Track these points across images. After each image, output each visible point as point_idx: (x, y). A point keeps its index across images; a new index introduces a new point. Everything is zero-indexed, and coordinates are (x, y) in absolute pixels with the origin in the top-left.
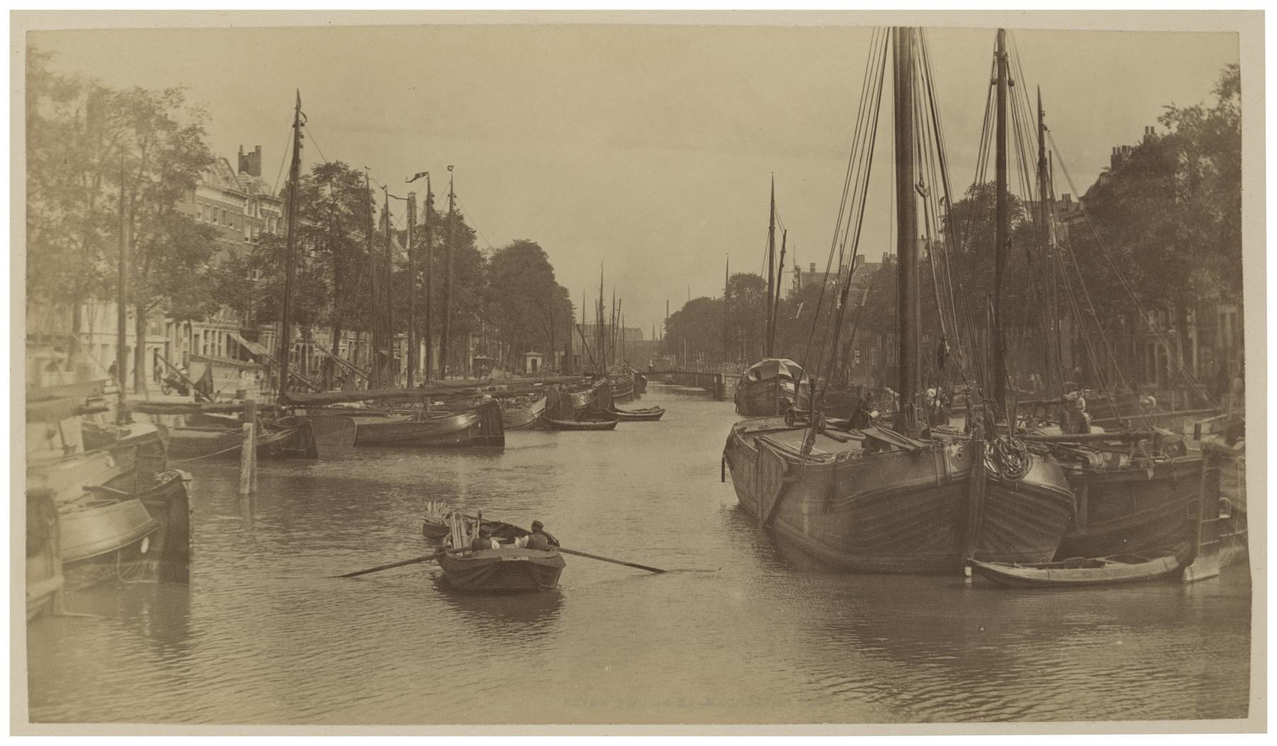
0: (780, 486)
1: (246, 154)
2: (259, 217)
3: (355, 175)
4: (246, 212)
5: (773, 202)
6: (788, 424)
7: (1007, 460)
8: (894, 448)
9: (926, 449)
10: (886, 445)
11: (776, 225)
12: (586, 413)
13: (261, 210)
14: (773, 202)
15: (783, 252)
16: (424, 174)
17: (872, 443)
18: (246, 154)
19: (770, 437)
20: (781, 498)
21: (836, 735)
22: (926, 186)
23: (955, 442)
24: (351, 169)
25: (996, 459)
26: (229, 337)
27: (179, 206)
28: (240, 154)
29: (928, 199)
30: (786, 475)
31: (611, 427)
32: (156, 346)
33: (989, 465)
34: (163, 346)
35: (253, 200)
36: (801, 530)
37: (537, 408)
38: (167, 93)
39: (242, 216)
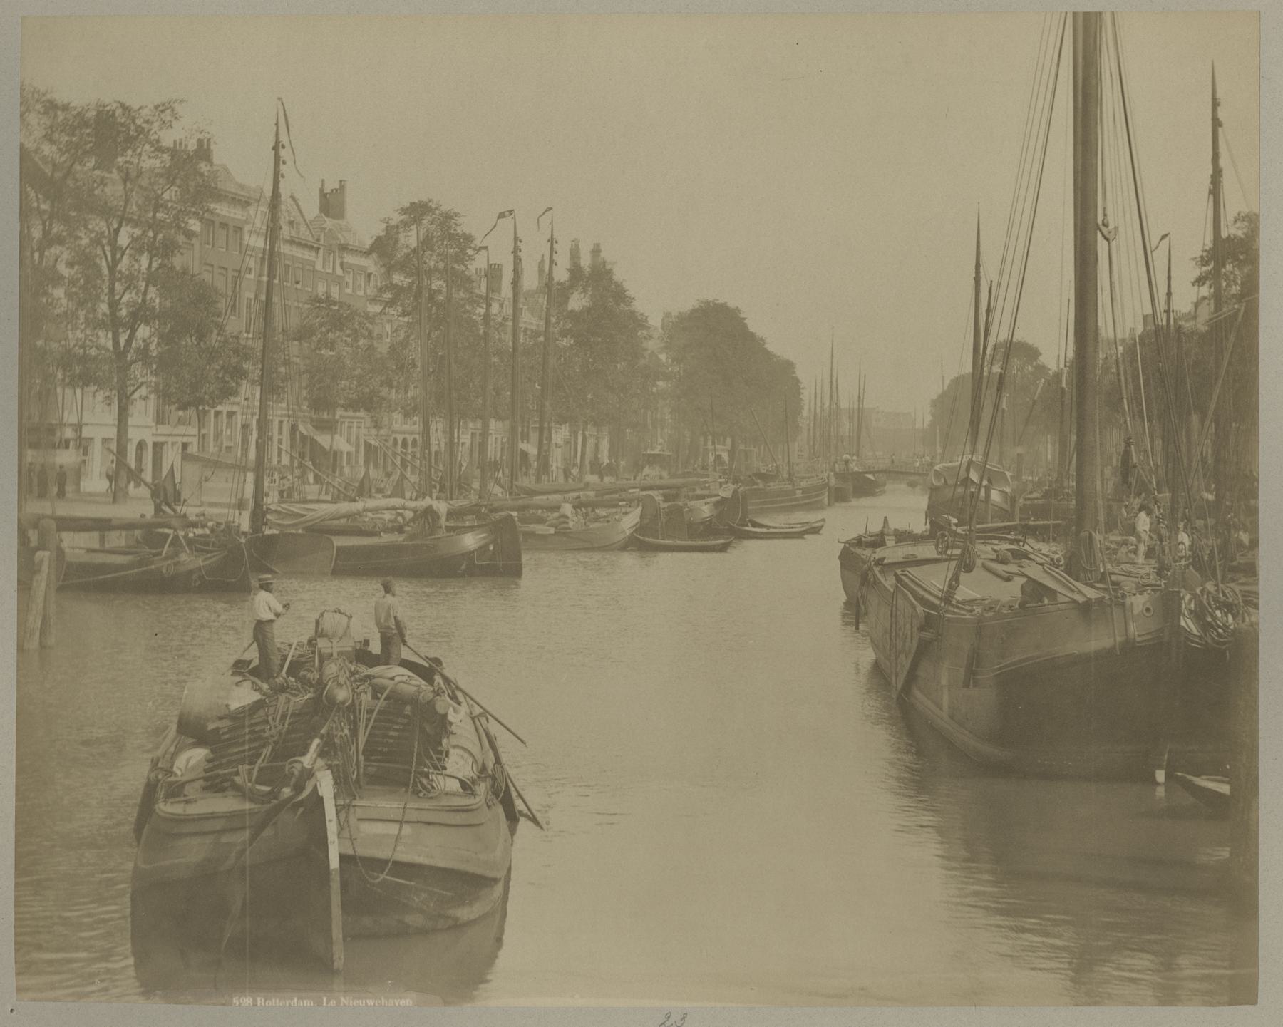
0: (915, 643)
1: (327, 190)
2: (339, 272)
3: (449, 216)
4: (319, 267)
5: (978, 242)
6: (939, 553)
7: (1215, 618)
8: (1061, 599)
9: (1100, 601)
10: (1052, 593)
11: (982, 274)
12: (708, 529)
13: (342, 264)
14: (978, 242)
15: (988, 311)
16: (511, 212)
17: (1035, 591)
18: (327, 190)
19: (914, 571)
20: (914, 666)
21: (1256, 652)
22: (1111, 226)
23: (1141, 589)
24: (444, 208)
25: (1199, 615)
26: (294, 428)
27: (177, 261)
28: (322, 190)
29: (1113, 243)
30: (922, 629)
31: (723, 548)
32: (185, 440)
33: (1188, 623)
34: (195, 441)
35: (330, 251)
36: (940, 707)
37: (629, 521)
38: (160, 108)
39: (314, 271)
